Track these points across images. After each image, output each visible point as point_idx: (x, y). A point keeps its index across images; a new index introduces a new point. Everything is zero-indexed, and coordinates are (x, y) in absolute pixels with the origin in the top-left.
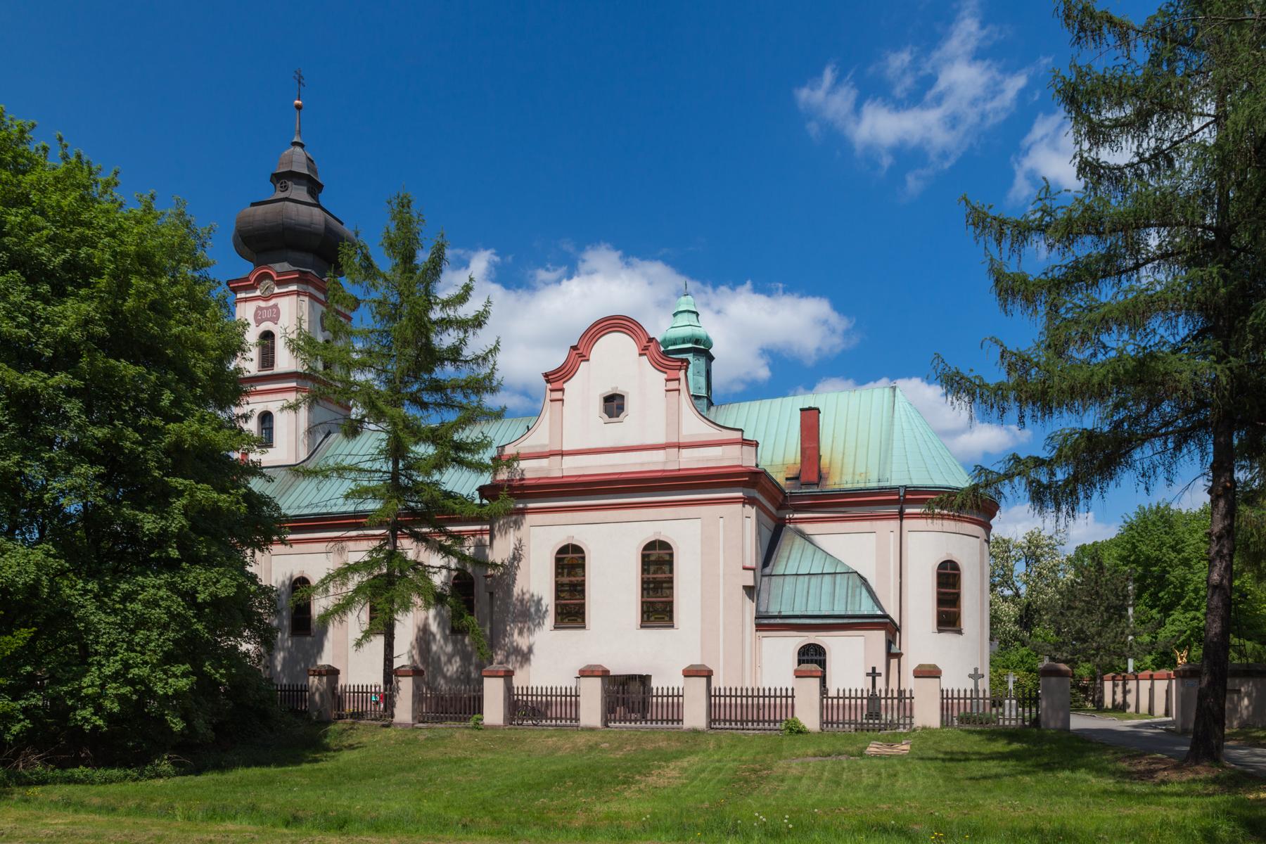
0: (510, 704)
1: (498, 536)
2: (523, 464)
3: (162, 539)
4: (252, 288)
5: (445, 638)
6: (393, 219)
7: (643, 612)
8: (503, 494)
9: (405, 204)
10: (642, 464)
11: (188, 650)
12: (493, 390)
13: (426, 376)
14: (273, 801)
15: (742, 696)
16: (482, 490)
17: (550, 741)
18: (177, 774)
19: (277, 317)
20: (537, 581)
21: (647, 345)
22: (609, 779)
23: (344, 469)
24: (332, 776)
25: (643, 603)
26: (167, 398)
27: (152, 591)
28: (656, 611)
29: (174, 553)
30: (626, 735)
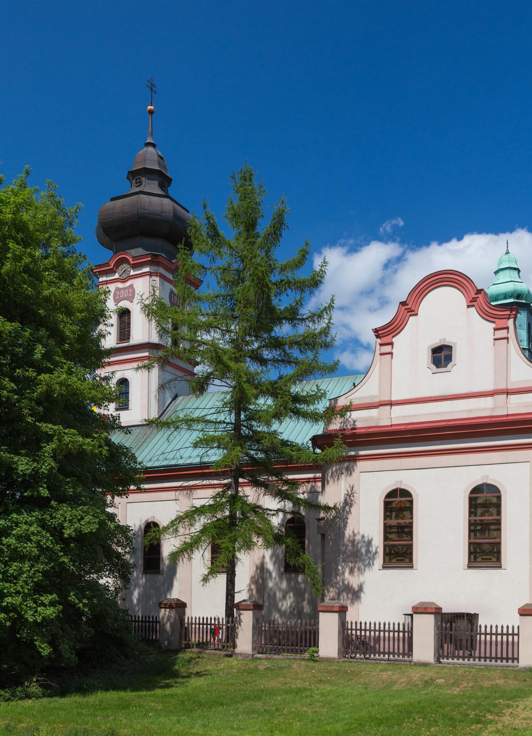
0: (343, 638)
1: (331, 482)
2: (355, 415)
3: (34, 479)
4: (112, 272)
5: (281, 575)
6: (237, 192)
7: (470, 553)
8: (338, 441)
9: (247, 178)
10: (470, 411)
11: (56, 581)
12: (327, 346)
13: (265, 336)
14: (131, 727)
15: (384, 631)
16: (316, 440)
17: (385, 675)
18: (44, 696)
19: (133, 297)
20: (367, 523)
21: (476, 297)
22: (459, 717)
23: (193, 420)
24: (183, 702)
25: (470, 544)
26: (39, 351)
27: (25, 527)
28: (483, 552)
29: (44, 492)
30: (460, 672)
